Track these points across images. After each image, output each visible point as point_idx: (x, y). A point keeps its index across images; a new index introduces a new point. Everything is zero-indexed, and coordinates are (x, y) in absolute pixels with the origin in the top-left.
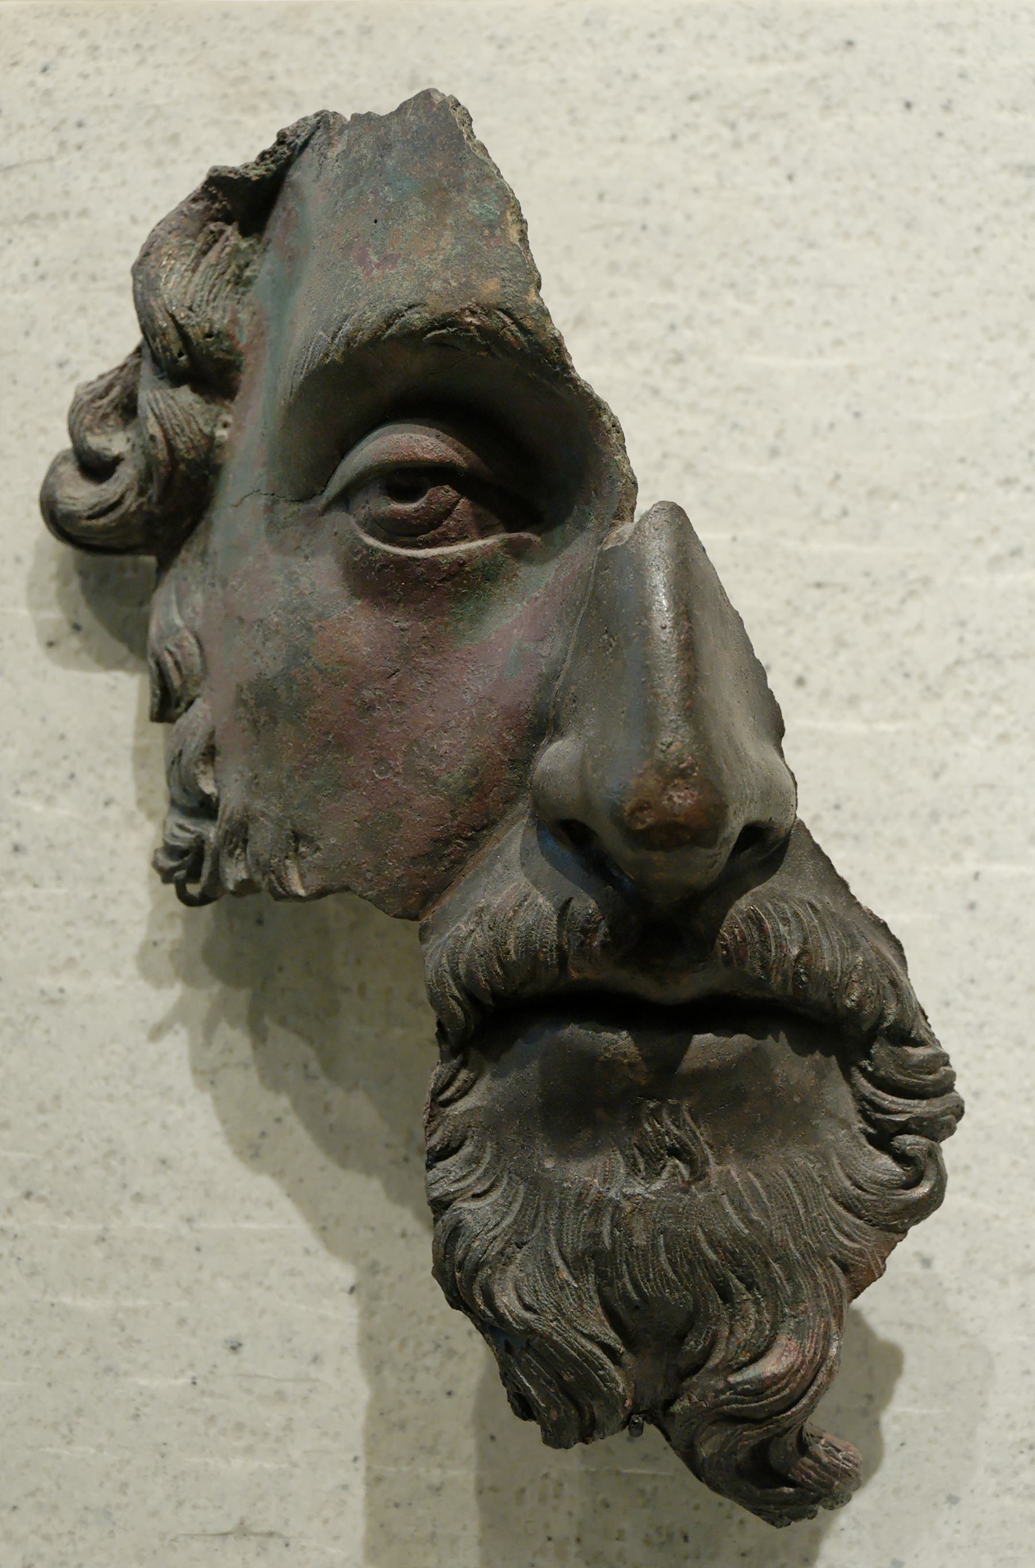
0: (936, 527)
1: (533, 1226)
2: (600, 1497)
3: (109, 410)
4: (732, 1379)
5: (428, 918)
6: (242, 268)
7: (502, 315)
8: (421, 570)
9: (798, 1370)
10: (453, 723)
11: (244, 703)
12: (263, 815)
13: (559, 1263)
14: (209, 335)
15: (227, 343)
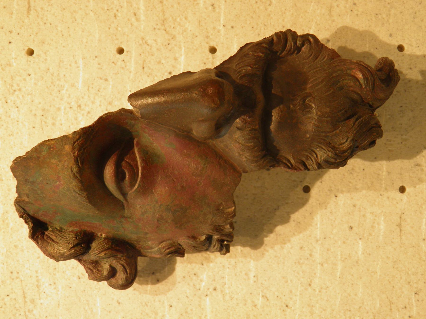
0: (128, 36)
4: (364, 87)
5: (241, 170)
6: (57, 230)
8: (145, 172)
10: (187, 163)
11: (181, 226)
12: (212, 220)
13: (334, 132)
15: (79, 233)
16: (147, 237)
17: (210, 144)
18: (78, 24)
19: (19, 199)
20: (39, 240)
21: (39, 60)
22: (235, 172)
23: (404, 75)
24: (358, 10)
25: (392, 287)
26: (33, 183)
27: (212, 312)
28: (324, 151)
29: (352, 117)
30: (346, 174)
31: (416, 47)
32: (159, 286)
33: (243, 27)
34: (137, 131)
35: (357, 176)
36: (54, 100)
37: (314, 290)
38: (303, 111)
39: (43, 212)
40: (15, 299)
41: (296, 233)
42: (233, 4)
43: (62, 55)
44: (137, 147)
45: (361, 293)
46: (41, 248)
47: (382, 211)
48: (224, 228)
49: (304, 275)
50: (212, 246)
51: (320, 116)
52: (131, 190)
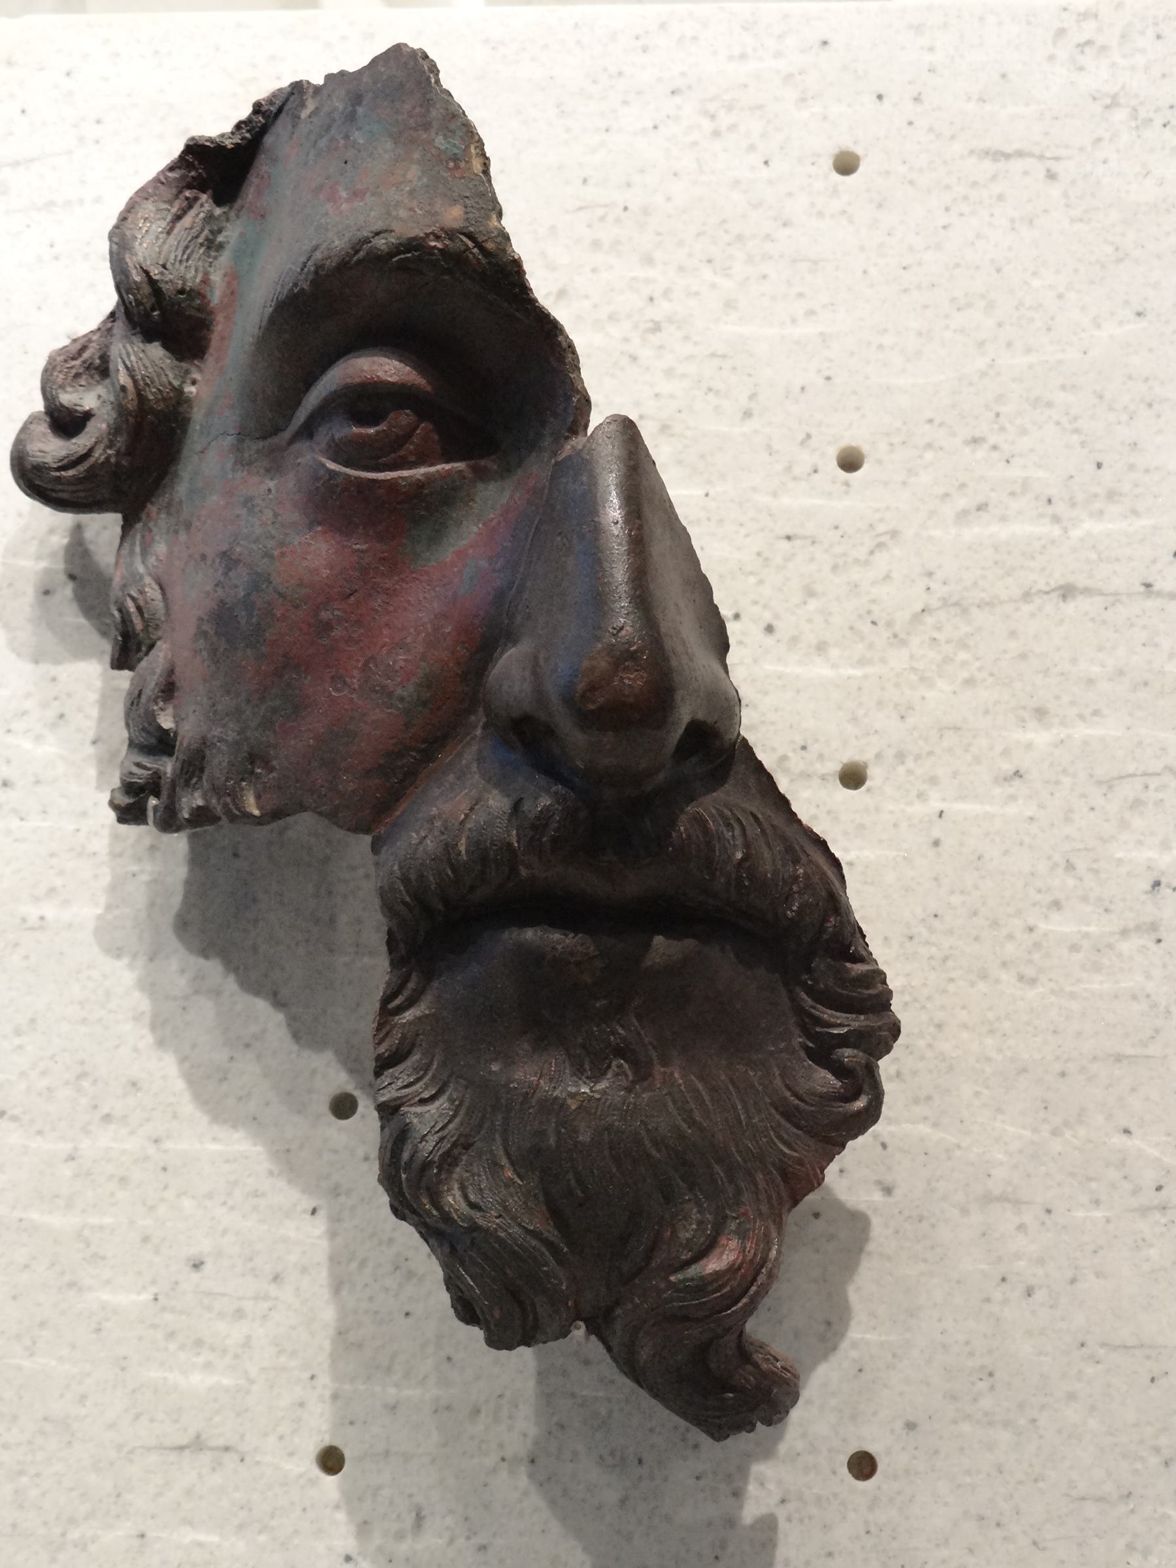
0: (904, 483)
1: (480, 1126)
2: (555, 1419)
3: (81, 371)
4: (672, 1278)
7: (464, 239)
9: (739, 1268)
10: (409, 640)
11: (205, 634)
13: (504, 1161)
14: (182, 291)
18: (947, 316)
22: (377, 803)
24: (1005, 1302)
26: (351, 117)
31: (866, 1522)
33: (936, 879)
35: (387, 1289)
40: (11, 134)
42: (1021, 844)
46: (157, 181)
48: (195, 789)
49: (40, 1094)
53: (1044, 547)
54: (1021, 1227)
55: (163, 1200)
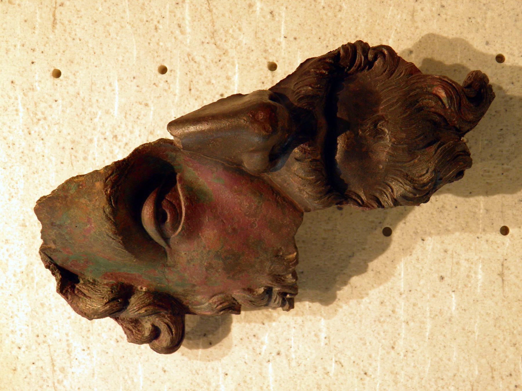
0: (171, 52)
1: (401, 171)
2: (489, 158)
4: (447, 107)
5: (303, 209)
6: (90, 282)
8: (189, 212)
10: (239, 201)
11: (233, 275)
12: (270, 268)
13: (412, 162)
14: (112, 292)
15: (115, 286)
16: (195, 291)
17: (265, 178)
18: (112, 39)
19: (44, 246)
20: (68, 294)
21: (67, 83)
22: (296, 211)
23: (504, 91)
24: (446, 14)
25: (493, 350)
26: (60, 226)
27: (276, 381)
28: (401, 184)
29: (434, 144)
30: (435, 213)
32: (212, 350)
33: (307, 39)
34: (179, 165)
35: (448, 214)
36: (85, 130)
37: (398, 354)
38: (374, 138)
39: (73, 261)
40: (42, 367)
41: (375, 285)
43: (95, 76)
44: (179, 183)
45: (456, 357)
46: (71, 304)
47: (480, 258)
48: (285, 278)
50: (273, 300)
51: (394, 143)
52: (174, 233)
53: (193, 5)
54: (422, 10)
55: (421, 291)
